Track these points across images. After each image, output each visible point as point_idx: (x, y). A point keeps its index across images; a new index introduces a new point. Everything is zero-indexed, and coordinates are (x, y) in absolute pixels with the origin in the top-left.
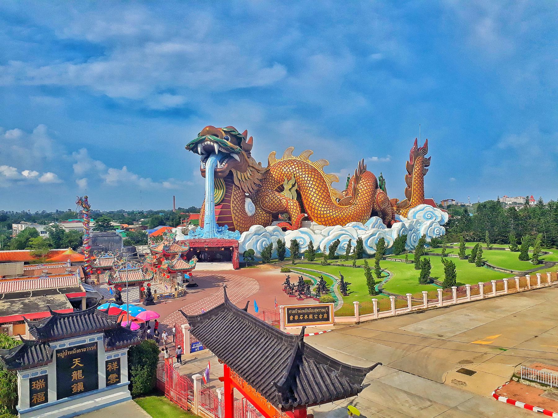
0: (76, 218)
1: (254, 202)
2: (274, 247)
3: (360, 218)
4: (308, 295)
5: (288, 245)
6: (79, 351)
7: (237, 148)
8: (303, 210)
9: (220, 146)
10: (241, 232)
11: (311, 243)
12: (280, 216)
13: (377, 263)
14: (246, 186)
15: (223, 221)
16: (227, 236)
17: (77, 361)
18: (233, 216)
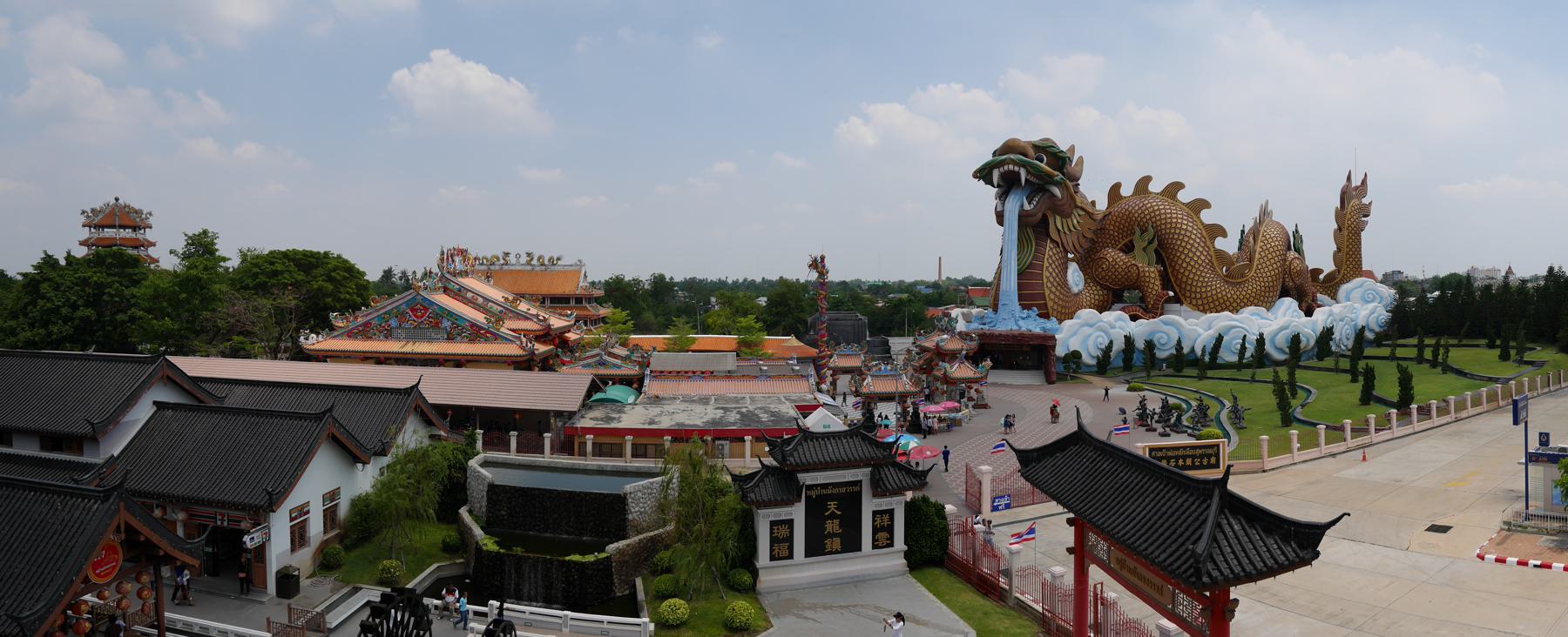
0: (513, 509)
1: (1083, 268)
2: (1115, 348)
3: (1265, 300)
4: (1177, 428)
5: (1140, 345)
6: (835, 491)
7: (1059, 176)
8: (1167, 284)
9: (1028, 172)
10: (1060, 321)
11: (1179, 342)
12: (1126, 294)
13: (1292, 374)
14: (1070, 240)
15: (1029, 297)
16: (1032, 325)
17: (832, 505)
18: (1047, 292)
